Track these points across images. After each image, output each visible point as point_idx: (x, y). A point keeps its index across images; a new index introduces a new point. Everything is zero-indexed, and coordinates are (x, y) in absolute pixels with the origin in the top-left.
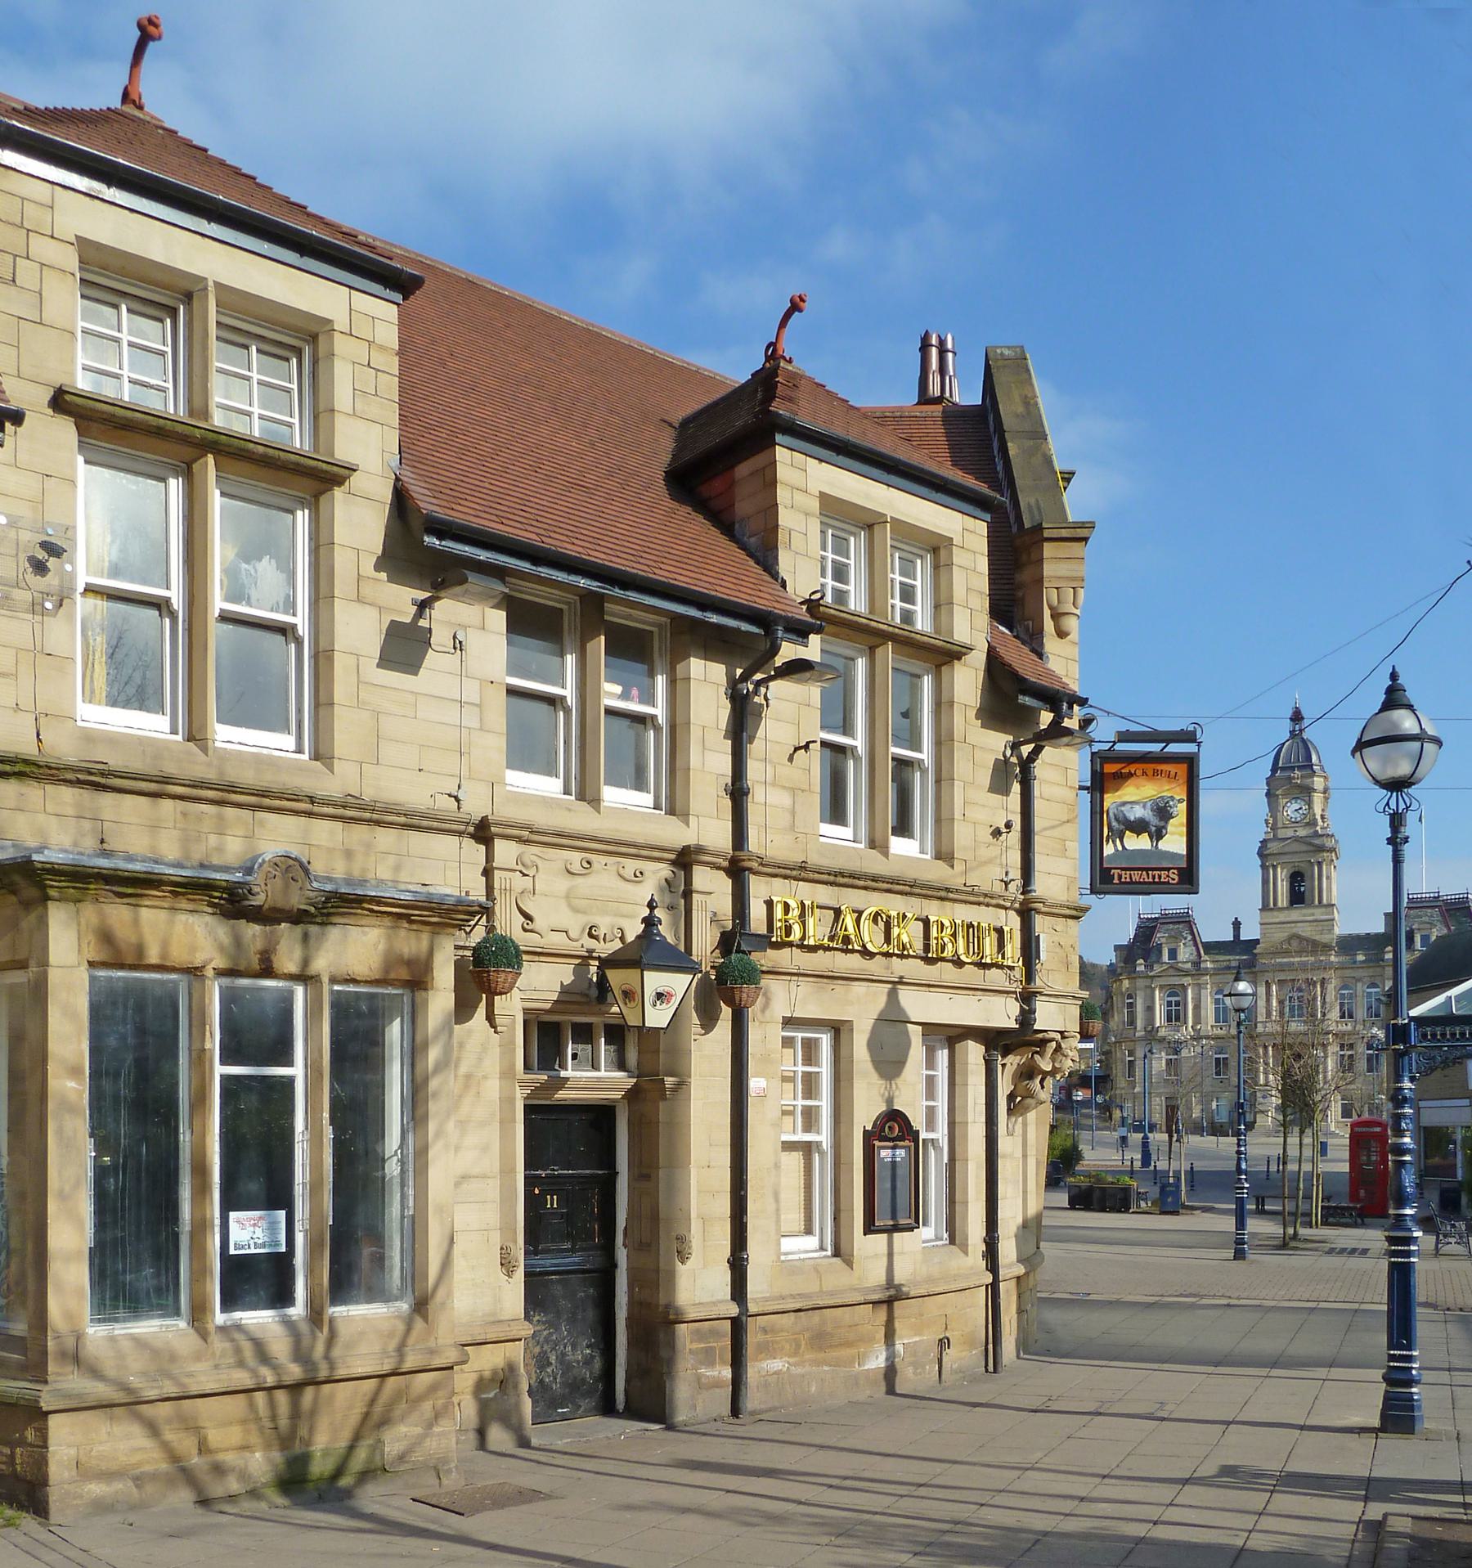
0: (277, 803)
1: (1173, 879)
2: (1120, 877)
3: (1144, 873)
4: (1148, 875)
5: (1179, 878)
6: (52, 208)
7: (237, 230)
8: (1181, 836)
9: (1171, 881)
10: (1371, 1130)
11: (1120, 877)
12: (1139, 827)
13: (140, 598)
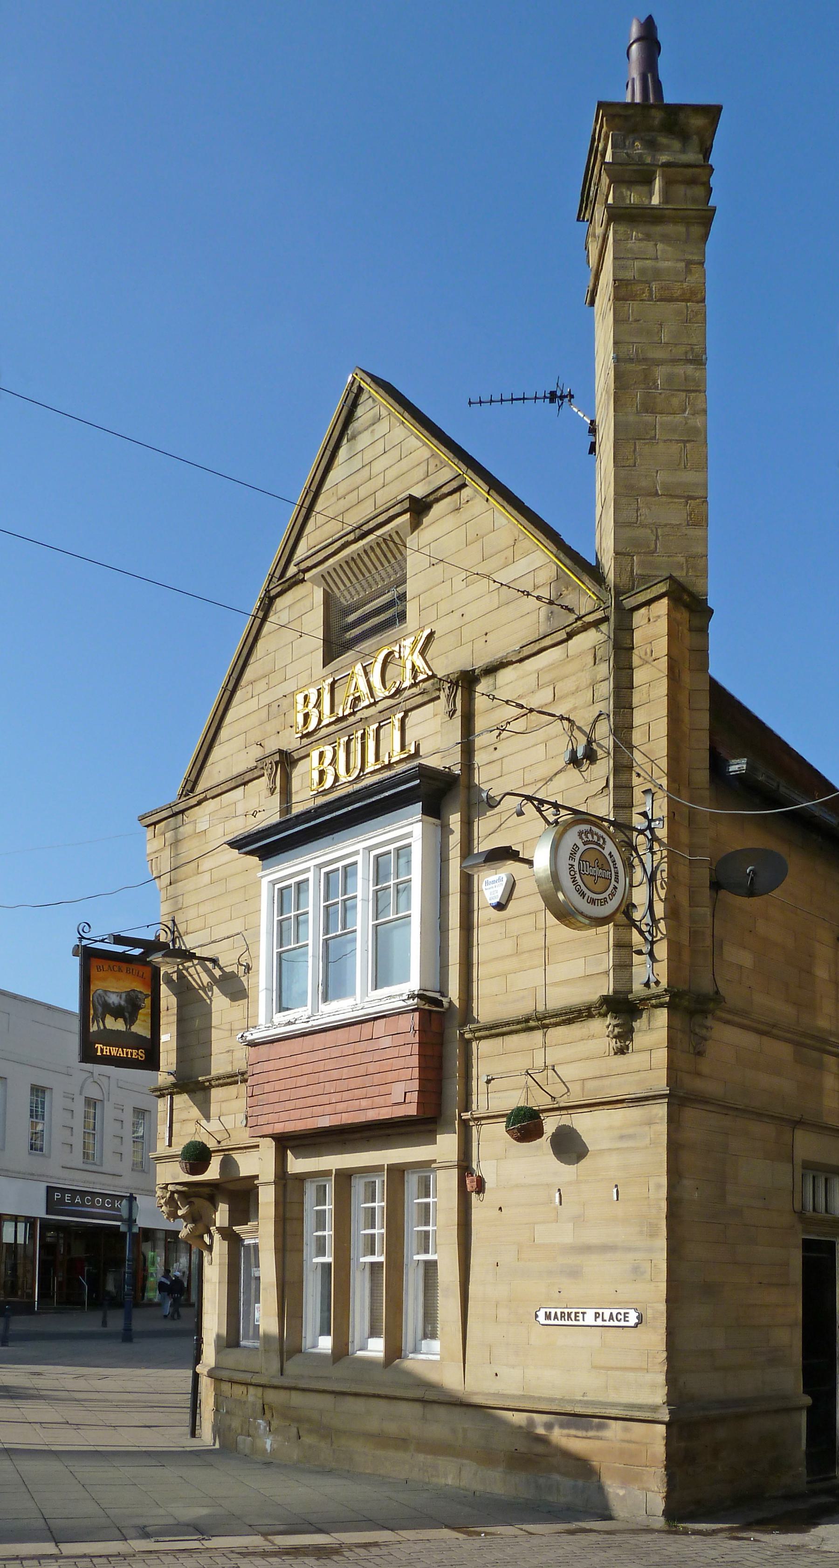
0: (505, 1029)
1: (142, 1057)
2: (102, 1050)
3: (120, 1049)
4: (123, 1051)
5: (145, 1056)
6: (651, 1050)
7: (410, 970)
8: (326, 1036)
9: (140, 1058)
10: (730, 1525)
11: (102, 1050)
12: (117, 1012)
13: (375, 982)
